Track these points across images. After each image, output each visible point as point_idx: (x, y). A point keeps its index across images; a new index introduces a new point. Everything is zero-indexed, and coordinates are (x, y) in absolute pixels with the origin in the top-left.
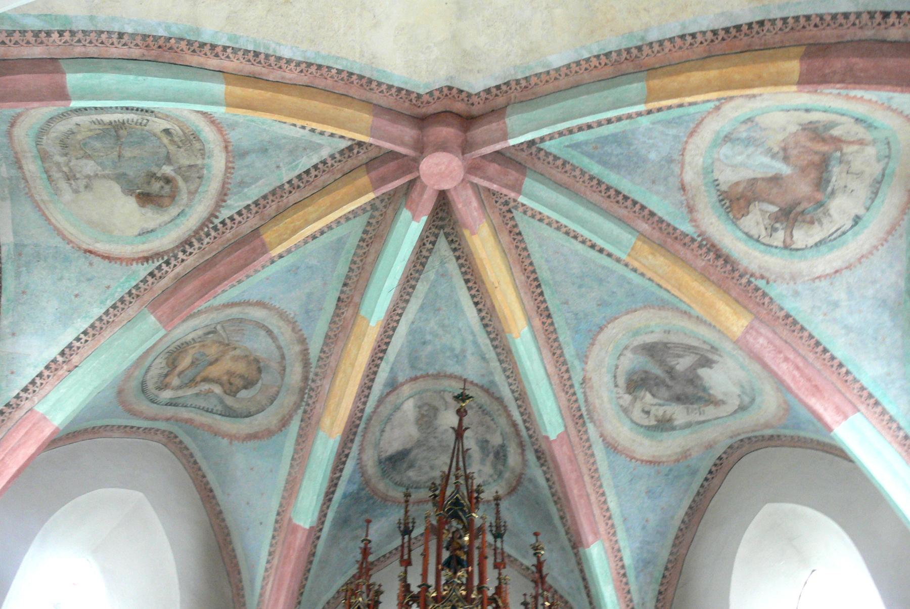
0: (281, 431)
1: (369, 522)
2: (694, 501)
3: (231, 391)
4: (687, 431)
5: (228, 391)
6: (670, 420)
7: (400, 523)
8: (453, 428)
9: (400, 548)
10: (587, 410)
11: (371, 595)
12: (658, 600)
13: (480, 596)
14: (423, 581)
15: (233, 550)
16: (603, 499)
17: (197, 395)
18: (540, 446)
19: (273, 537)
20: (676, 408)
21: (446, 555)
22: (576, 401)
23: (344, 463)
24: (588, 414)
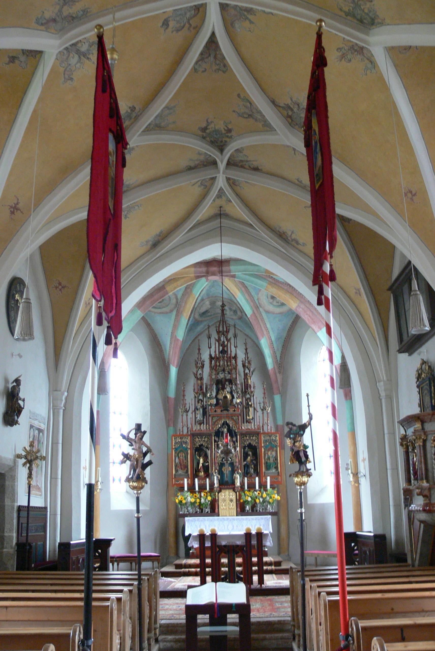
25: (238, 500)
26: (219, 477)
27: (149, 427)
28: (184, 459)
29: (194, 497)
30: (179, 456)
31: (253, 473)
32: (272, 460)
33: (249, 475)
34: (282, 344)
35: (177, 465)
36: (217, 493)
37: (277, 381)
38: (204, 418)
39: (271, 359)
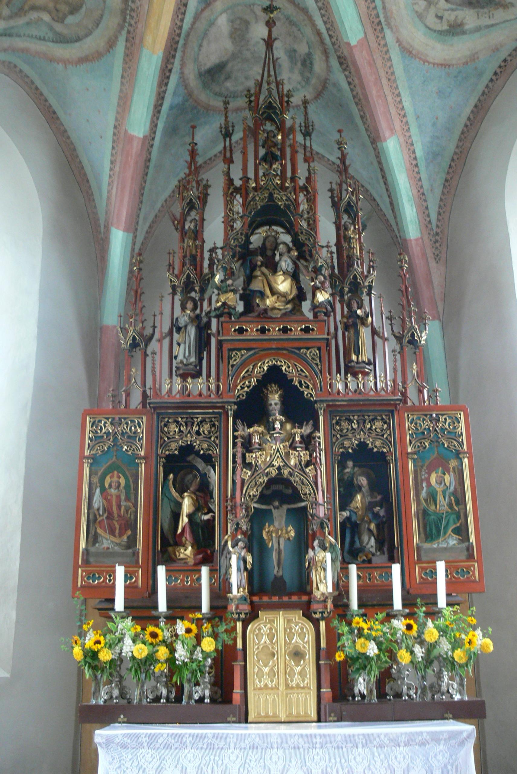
0: (109, 52)
1: (194, 127)
2: (479, 100)
3: (58, 18)
4: (477, 35)
5: (56, 18)
6: (461, 25)
7: (221, 127)
8: (264, 40)
9: (223, 152)
10: (384, 17)
11: (200, 189)
12: (444, 186)
13: (293, 184)
14: (243, 173)
15: (80, 162)
16: (398, 99)
17: (28, 24)
18: (342, 53)
19: (113, 148)
20: (467, 12)
21: (262, 152)
22: (375, 8)
23: (168, 78)
24: (385, 21)
25: (323, 654)
26: (249, 559)
27: (30, 405)
28: (123, 497)
29: (148, 638)
30: (107, 486)
31: (373, 550)
32: (442, 503)
33: (362, 557)
34: (444, 177)
35: (95, 519)
36: (239, 625)
37: (430, 282)
38: (201, 359)
39: (415, 210)
